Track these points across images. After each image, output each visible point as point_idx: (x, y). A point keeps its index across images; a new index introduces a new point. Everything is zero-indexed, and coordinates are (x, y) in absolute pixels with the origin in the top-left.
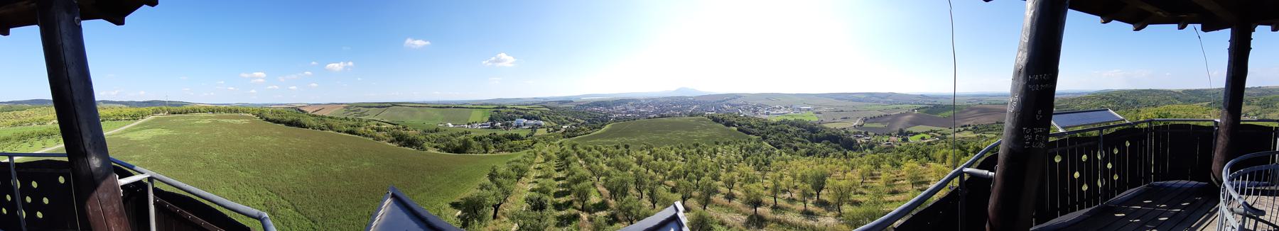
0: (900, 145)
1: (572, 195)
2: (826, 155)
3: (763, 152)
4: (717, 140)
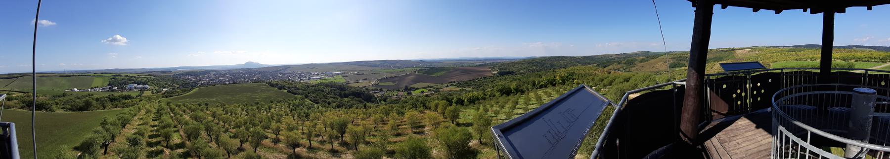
0: (406, 98)
2: (351, 107)
3: (305, 107)
4: (272, 99)
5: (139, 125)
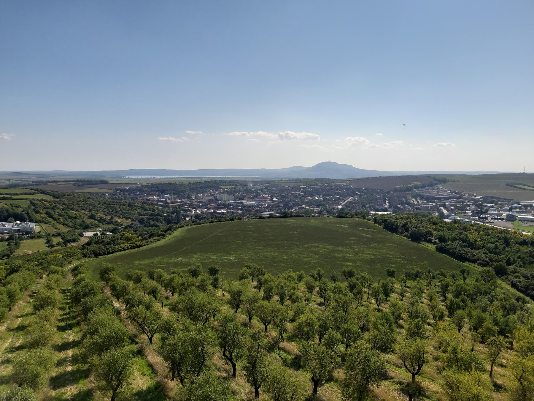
1: (92, 378)
4: (392, 267)
5: (12, 350)
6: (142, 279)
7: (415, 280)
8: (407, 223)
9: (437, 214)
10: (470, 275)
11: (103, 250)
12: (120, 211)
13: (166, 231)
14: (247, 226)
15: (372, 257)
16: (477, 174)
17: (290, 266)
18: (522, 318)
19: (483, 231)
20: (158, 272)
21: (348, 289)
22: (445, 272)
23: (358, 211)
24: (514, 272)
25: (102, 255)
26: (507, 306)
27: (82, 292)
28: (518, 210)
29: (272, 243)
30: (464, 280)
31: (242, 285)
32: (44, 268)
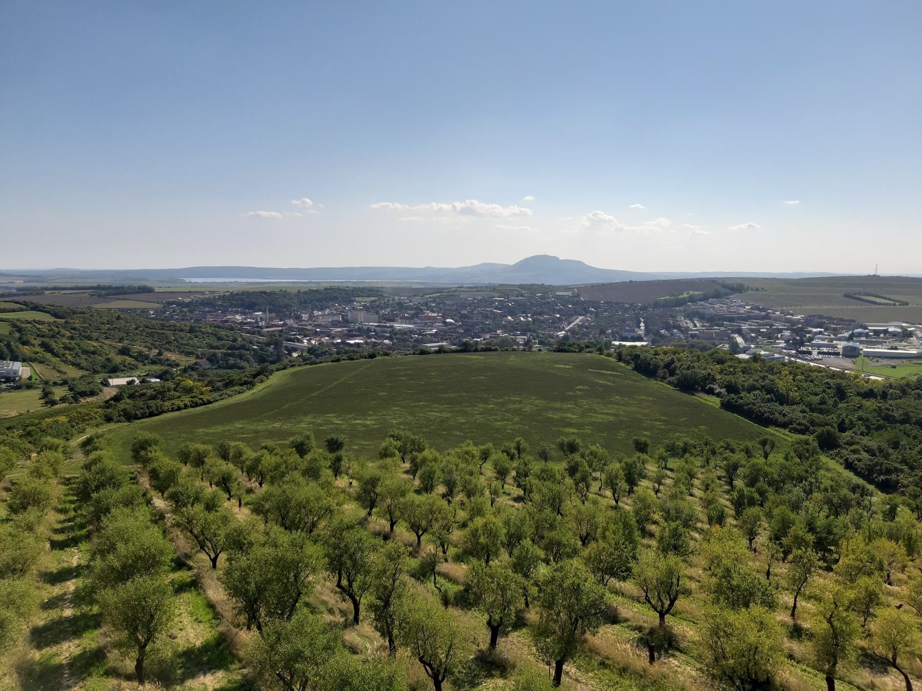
3: (817, 496)
4: (645, 436)
6: (206, 459)
7: (682, 457)
8: (672, 361)
9: (727, 346)
10: (775, 449)
11: (142, 409)
12: (174, 340)
13: (255, 376)
14: (399, 367)
15: (611, 418)
16: (796, 278)
17: (469, 435)
18: (859, 519)
19: (802, 374)
20: (234, 447)
21: (566, 474)
22: (733, 443)
23: (592, 340)
24: (850, 444)
25: (140, 418)
26: (835, 500)
27: (94, 481)
28: (863, 339)
29: (441, 395)
30: (766, 456)
31: (385, 467)
32: (34, 440)
